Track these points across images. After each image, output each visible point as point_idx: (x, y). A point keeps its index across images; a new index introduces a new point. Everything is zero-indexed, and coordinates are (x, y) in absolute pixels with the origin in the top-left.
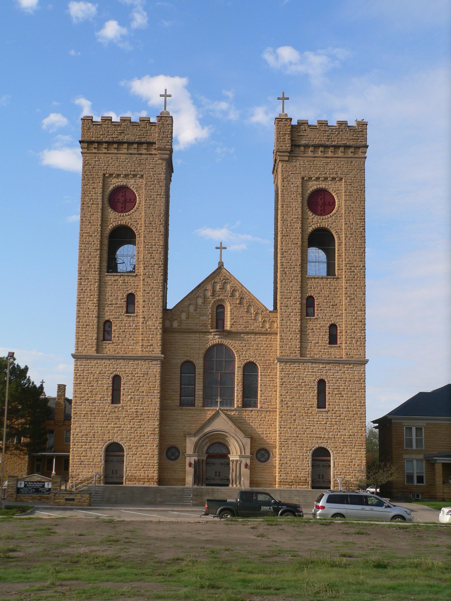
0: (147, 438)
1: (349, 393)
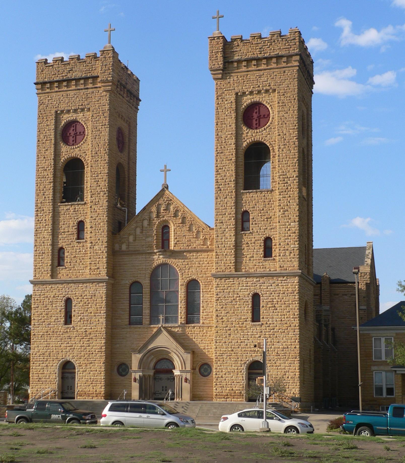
0: (95, 356)
1: (283, 306)
